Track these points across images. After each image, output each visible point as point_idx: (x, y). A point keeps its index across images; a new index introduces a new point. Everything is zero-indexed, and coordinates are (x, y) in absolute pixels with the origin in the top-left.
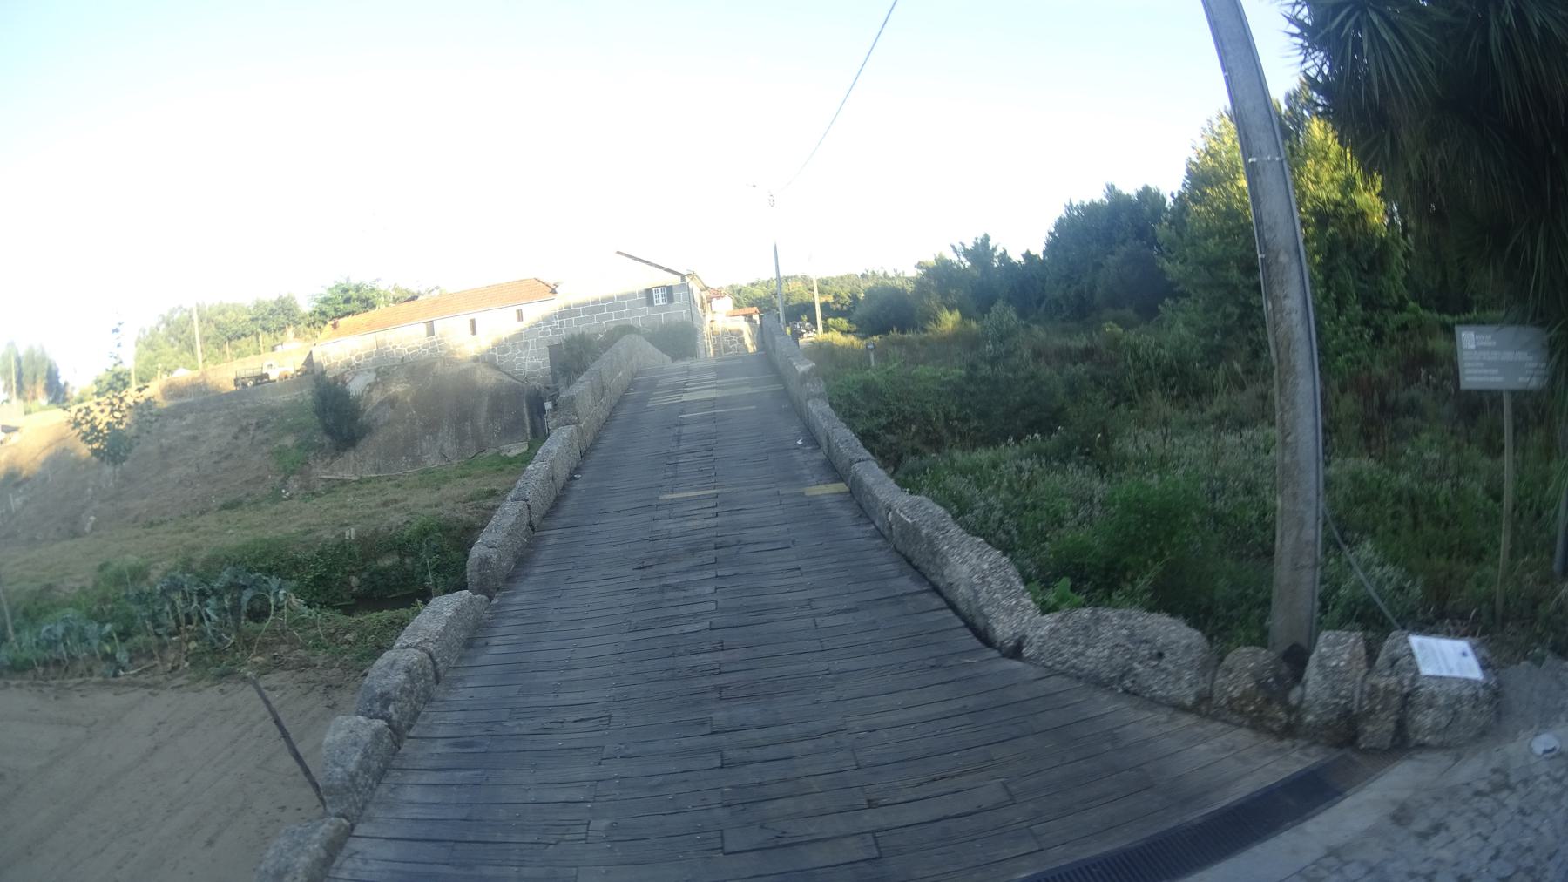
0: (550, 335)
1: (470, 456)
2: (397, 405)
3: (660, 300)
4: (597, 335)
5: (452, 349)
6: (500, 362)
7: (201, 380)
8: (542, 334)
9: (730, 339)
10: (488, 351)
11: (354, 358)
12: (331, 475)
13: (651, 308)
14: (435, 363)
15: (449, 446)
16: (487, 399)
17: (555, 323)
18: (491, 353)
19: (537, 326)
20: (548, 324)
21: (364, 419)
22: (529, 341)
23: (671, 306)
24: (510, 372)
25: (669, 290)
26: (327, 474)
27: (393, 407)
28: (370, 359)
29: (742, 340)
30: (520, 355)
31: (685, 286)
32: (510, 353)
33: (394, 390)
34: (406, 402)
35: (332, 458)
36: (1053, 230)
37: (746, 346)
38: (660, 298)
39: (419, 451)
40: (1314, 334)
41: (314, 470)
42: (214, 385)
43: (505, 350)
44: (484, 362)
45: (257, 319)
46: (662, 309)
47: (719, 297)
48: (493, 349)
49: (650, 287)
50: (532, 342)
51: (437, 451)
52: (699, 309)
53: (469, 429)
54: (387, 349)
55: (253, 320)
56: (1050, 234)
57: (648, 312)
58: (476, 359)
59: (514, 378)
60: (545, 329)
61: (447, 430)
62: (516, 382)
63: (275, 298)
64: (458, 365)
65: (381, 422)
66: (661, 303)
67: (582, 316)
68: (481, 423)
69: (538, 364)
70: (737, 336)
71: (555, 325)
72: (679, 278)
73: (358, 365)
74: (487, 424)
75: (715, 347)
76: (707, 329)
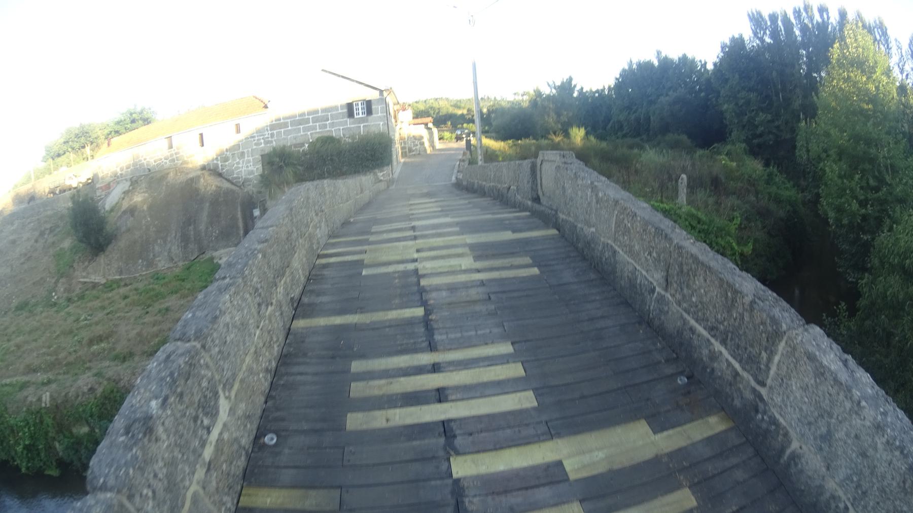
0: (263, 145)
1: (193, 259)
2: (136, 213)
3: (360, 113)
4: (302, 145)
5: (186, 159)
6: (222, 169)
7: (32, 190)
8: (256, 144)
9: (413, 142)
10: (213, 160)
11: (118, 170)
12: (87, 278)
13: (352, 120)
14: (168, 174)
15: (176, 250)
16: (208, 204)
17: (267, 134)
18: (215, 162)
19: (252, 137)
20: (261, 136)
21: (109, 228)
22: (246, 151)
23: (370, 118)
24: (230, 178)
25: (368, 106)
26: (84, 277)
27: (132, 215)
28: (129, 170)
29: (422, 144)
30: (238, 163)
31: (383, 101)
32: (230, 161)
33: (135, 200)
34: (144, 210)
35: (89, 262)
36: (618, 76)
37: (425, 148)
38: (360, 111)
39: (152, 255)
40: (538, 173)
41: (76, 273)
42: (40, 193)
43: (226, 159)
44: (210, 170)
45: (68, 142)
46: (362, 120)
47: (404, 110)
48: (217, 159)
49: (351, 102)
50: (248, 151)
51: (166, 254)
52: (393, 120)
53: (192, 233)
54: (141, 161)
55: (65, 143)
56: (617, 79)
57: (349, 124)
58: (203, 168)
59: (232, 183)
60: (258, 140)
61: (174, 235)
62: (233, 187)
63: (78, 126)
64: (187, 174)
65: (124, 229)
66: (361, 115)
67: (290, 128)
68: (202, 227)
69: (252, 171)
70: (419, 140)
71: (267, 136)
72: (377, 93)
73: (121, 174)
74: (207, 228)
75: (402, 148)
76: (397, 138)
